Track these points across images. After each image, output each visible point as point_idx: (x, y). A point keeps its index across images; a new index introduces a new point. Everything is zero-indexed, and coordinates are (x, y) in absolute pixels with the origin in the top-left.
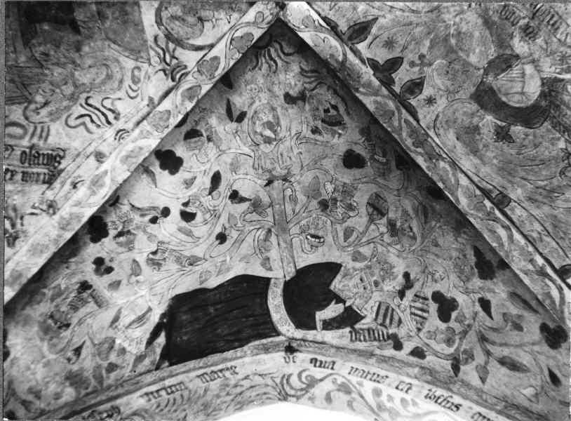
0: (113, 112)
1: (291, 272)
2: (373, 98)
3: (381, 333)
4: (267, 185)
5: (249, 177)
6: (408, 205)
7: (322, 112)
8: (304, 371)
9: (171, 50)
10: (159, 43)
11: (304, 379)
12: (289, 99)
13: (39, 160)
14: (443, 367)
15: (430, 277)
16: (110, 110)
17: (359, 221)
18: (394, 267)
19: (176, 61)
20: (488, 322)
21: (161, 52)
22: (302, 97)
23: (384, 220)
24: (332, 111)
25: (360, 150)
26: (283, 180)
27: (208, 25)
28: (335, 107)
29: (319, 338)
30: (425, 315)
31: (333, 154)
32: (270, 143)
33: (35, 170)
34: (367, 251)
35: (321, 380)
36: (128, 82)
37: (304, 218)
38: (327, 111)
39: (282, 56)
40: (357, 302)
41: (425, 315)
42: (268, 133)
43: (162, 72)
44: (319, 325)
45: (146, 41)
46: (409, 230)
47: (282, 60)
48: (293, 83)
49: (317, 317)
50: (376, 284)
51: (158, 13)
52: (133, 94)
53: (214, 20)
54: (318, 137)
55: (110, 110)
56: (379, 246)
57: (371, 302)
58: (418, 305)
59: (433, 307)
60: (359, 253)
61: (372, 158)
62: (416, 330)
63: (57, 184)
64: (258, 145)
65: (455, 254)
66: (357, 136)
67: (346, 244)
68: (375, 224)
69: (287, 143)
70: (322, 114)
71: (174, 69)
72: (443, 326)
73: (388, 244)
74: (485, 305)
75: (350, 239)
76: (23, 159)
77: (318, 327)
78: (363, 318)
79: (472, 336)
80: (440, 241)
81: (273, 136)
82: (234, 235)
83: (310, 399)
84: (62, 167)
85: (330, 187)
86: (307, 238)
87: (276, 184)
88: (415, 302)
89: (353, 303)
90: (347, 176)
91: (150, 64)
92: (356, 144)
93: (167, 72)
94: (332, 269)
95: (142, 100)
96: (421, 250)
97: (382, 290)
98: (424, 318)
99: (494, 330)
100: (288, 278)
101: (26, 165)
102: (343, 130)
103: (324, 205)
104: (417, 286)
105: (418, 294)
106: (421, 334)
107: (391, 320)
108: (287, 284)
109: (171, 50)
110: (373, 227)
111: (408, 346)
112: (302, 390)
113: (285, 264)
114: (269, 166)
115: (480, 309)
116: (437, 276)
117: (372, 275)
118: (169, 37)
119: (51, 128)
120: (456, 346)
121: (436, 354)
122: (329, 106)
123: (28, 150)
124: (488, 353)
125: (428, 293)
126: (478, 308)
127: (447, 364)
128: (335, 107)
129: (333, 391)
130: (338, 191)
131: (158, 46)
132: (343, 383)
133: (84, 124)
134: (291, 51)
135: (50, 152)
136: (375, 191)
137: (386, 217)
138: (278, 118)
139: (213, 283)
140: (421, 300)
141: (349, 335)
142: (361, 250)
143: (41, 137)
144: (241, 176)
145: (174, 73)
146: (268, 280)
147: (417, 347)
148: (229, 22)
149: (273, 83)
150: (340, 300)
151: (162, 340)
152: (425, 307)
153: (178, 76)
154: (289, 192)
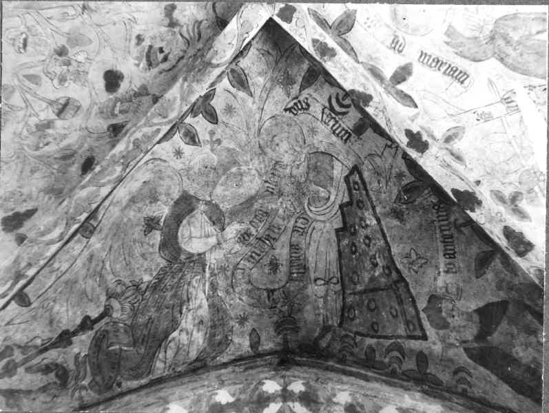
6: (72, 139)
17: (50, 90)
25: (124, 87)
38: (161, 50)
68: (47, 107)
70: (157, 45)
73: (26, 123)
85: (81, 58)
86: (22, 34)
128: (165, 59)
137: (56, 117)
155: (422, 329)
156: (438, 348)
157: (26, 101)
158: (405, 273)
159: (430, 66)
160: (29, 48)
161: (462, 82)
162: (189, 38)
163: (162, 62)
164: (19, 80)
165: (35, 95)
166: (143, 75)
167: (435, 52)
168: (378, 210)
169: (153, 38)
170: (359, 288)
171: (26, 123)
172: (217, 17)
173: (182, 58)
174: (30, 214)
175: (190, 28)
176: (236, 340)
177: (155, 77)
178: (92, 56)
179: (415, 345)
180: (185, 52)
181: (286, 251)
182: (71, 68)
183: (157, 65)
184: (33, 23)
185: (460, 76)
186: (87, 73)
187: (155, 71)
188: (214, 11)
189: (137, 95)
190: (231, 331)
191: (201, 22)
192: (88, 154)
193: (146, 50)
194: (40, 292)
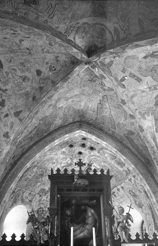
0: (53, 16)
2: (60, 85)
4: (27, 48)
10: (77, 25)
12: (57, 57)
16: (54, 14)
22: (57, 61)
24: (54, 69)
27: (81, 40)
28: (55, 70)
34: (10, 76)
36: (63, 17)
38: (54, 67)
42: (45, 50)
45: (77, 20)
51: (86, 23)
52: (59, 21)
54: (45, 64)
55: (54, 14)
60: (9, 74)
61: (41, 79)
65: (18, 104)
66: (46, 75)
69: (42, 55)
70: (53, 65)
73: (14, 83)
85: (29, 65)
86: (9, 58)
91: (69, 23)
103: (22, 64)
104: (4, 94)
109: (74, 30)
110: (19, 78)
118: (79, 28)
125: (4, 98)
133: (49, 7)
134: (72, 59)
136: (30, 78)
138: (50, 53)
153: (66, 34)
155: (115, 127)
156: (118, 132)
157: (13, 76)
158: (114, 117)
159: (132, 77)
160: (12, 62)
161: (140, 82)
163: (54, 70)
164: (10, 70)
165: (15, 75)
167: (134, 73)
168: (110, 105)
169: (51, 63)
170: (101, 115)
171: (14, 83)
172: (71, 61)
173: (60, 70)
174: (21, 112)
176: (69, 120)
179: (113, 130)
180: (61, 69)
181: (84, 104)
182: (26, 68)
185: (139, 80)
189: (46, 78)
190: (68, 118)
191: (66, 62)
192: (34, 95)
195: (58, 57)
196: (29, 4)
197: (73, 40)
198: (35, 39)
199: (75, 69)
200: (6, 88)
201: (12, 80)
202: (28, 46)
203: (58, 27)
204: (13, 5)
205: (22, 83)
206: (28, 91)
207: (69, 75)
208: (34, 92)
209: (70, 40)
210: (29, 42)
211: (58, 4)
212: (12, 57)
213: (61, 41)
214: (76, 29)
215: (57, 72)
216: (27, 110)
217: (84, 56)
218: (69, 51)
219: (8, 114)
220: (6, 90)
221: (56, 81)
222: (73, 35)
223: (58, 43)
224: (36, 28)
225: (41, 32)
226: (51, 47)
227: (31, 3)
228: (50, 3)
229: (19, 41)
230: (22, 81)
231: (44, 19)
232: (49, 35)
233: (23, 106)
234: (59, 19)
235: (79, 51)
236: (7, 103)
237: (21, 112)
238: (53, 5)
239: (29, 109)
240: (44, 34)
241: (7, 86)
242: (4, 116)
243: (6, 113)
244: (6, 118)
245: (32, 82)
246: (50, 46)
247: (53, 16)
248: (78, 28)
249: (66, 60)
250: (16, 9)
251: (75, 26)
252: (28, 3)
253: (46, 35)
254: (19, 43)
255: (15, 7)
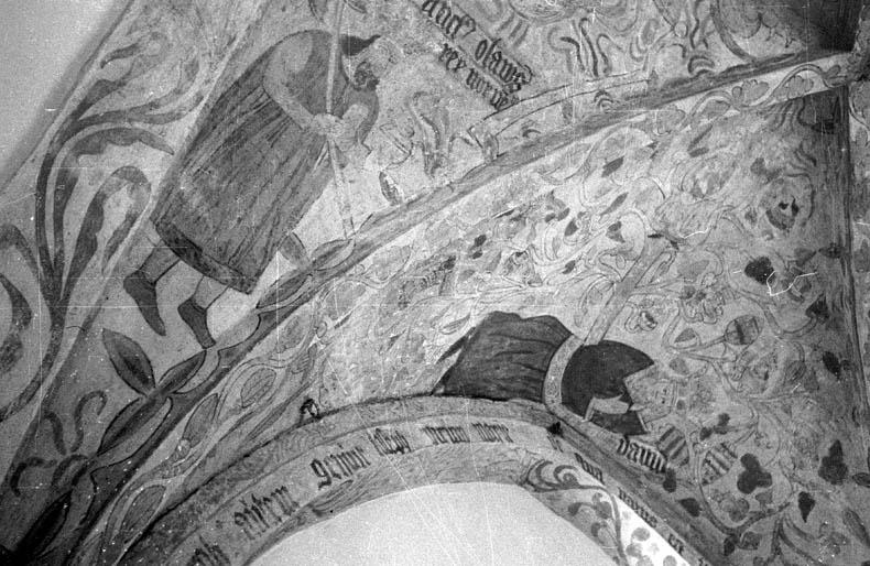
1: (595, 339)
3: (656, 461)
4: (653, 236)
5: (643, 217)
6: (784, 352)
7: (777, 203)
8: (570, 467)
9: (707, 30)
11: (561, 475)
13: (497, 65)
14: (713, 537)
15: (754, 436)
16: (603, 55)
17: (709, 332)
18: (714, 401)
19: (705, 49)
20: (798, 521)
21: (694, 23)
22: (772, 176)
23: (739, 349)
25: (778, 268)
26: (672, 242)
27: (763, 32)
28: (795, 209)
29: (582, 428)
30: (722, 471)
31: (745, 251)
32: (694, 196)
33: (487, 78)
34: (693, 365)
35: (582, 487)
37: (657, 293)
39: (795, 119)
40: (647, 411)
41: (722, 471)
42: (704, 186)
43: (680, 49)
44: (589, 413)
46: (763, 376)
47: (791, 124)
48: (777, 154)
49: (591, 404)
50: (680, 405)
52: (637, 55)
53: (773, 30)
54: (747, 225)
55: (603, 55)
56: (712, 369)
57: (663, 422)
58: (720, 456)
59: (738, 468)
62: (701, 480)
63: (507, 114)
64: (682, 190)
65: (804, 433)
66: (790, 253)
67: (675, 345)
68: (726, 346)
69: (710, 209)
70: (775, 205)
71: (697, 57)
72: (738, 495)
73: (725, 374)
74: (806, 503)
75: (683, 343)
76: (481, 51)
77: (587, 416)
78: (644, 433)
79: (768, 525)
80: (796, 410)
81: (704, 191)
82: (580, 268)
83: (551, 498)
84: (520, 94)
85: (710, 280)
86: (641, 315)
87: (662, 242)
88: (719, 451)
89: (642, 410)
90: (739, 280)
91: (672, 29)
92: (780, 256)
93: (687, 54)
94: (642, 361)
95: (644, 69)
96: (762, 404)
97: (684, 416)
98: (718, 473)
99: (800, 533)
100: (587, 344)
101: (480, 62)
102: (780, 235)
104: (730, 437)
105: (727, 445)
106: (705, 489)
107: (677, 454)
108: (582, 349)
109: (707, 30)
110: (720, 346)
111: (682, 493)
112: (549, 484)
113: (596, 326)
114: (672, 219)
115: (797, 503)
116: (763, 441)
117: (682, 393)
119: (531, 29)
120: (742, 523)
121: (712, 519)
122: (790, 203)
123: (490, 43)
124: (777, 551)
125: (741, 451)
126: (795, 501)
127: (722, 537)
128: (795, 209)
129: (586, 504)
130: (714, 289)
131: (695, 13)
132: (606, 503)
133: (568, 51)
135: (515, 65)
137: (744, 346)
138: (728, 178)
139: (527, 313)
140: (726, 453)
141: (619, 444)
142: (688, 360)
143: (513, 35)
144: (638, 212)
145: (695, 61)
146: (570, 334)
147: (694, 500)
148: (787, 46)
149: (759, 141)
150: (627, 398)
151: (454, 358)
152: (727, 463)
153: (698, 69)
154: (666, 257)
160: (656, 319)
162: (802, 172)
166: (789, 240)
169: (763, 203)
173: (814, 193)
175: (795, 161)
177: (801, 233)
178: (719, 271)
182: (708, 297)
183: (793, 220)
184: (641, 298)
186: (729, 286)
187: (796, 228)
188: (805, 124)
189: (801, 263)
191: (801, 146)
192: (819, 354)
193: (767, 219)
194: (775, 421)
195: (760, 162)
196: (510, 98)
197: (737, 61)
198: (643, 187)
199: (853, 132)
200: (721, 412)
201: (711, 371)
202: (648, 228)
203: (653, 75)
204: (473, 142)
205: (745, 353)
206: (787, 361)
207: (857, 171)
208: (811, 345)
209: (730, 70)
210: (638, 212)
211: (584, 19)
212: (643, 305)
213: (702, 95)
214: (711, 22)
215: (813, 208)
216: (851, 427)
217: (828, 63)
218: (764, 98)
219: (802, 494)
220: (725, 418)
221: (840, 239)
222: (723, 47)
223: (700, 110)
224: (587, 135)
225: (610, 133)
226: (707, 156)
227: (512, 91)
228: (563, 39)
229: (612, 238)
230: (742, 347)
231: (591, 97)
232: (643, 117)
233: (822, 423)
234: (631, 52)
235: (792, 68)
236: (764, 459)
237: (837, 449)
238: (573, 36)
239: (854, 417)
240: (627, 130)
241: (713, 404)
242: (799, 515)
243: (796, 495)
244: (812, 513)
245: (771, 319)
246: (699, 158)
247: (606, 60)
248: (713, 14)
249: (795, 142)
250: (489, 143)
251: (698, 21)
252: (506, 99)
253: (636, 126)
254: (614, 244)
255: (482, 141)
